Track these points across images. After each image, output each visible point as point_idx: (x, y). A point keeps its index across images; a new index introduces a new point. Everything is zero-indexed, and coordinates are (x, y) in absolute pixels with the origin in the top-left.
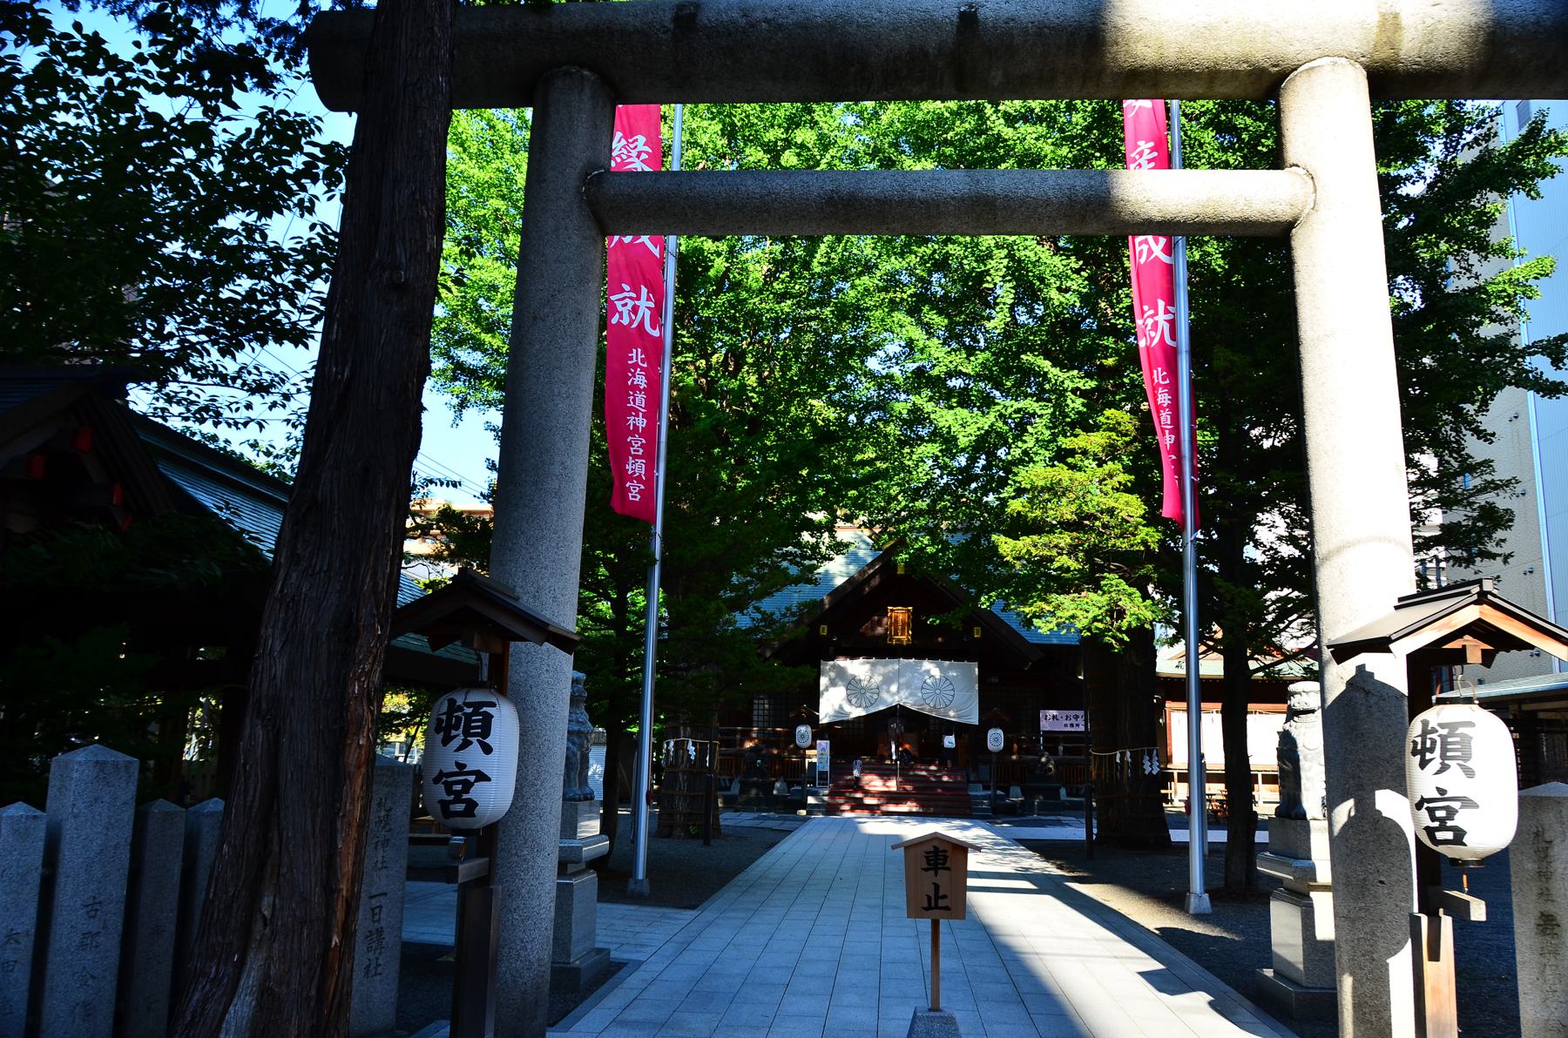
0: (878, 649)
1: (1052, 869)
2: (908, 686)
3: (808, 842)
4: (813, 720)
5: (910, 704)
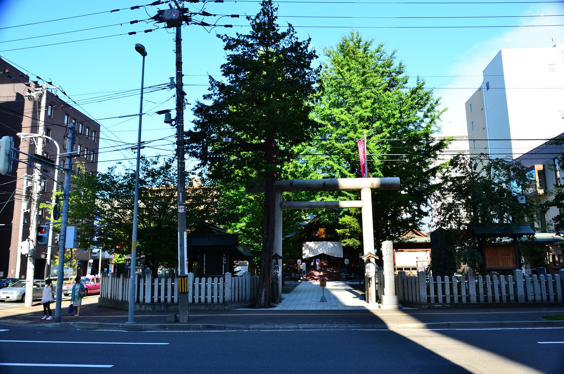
0: (317, 239)
1: (351, 288)
2: (325, 248)
3: (302, 285)
4: (301, 258)
5: (325, 253)
